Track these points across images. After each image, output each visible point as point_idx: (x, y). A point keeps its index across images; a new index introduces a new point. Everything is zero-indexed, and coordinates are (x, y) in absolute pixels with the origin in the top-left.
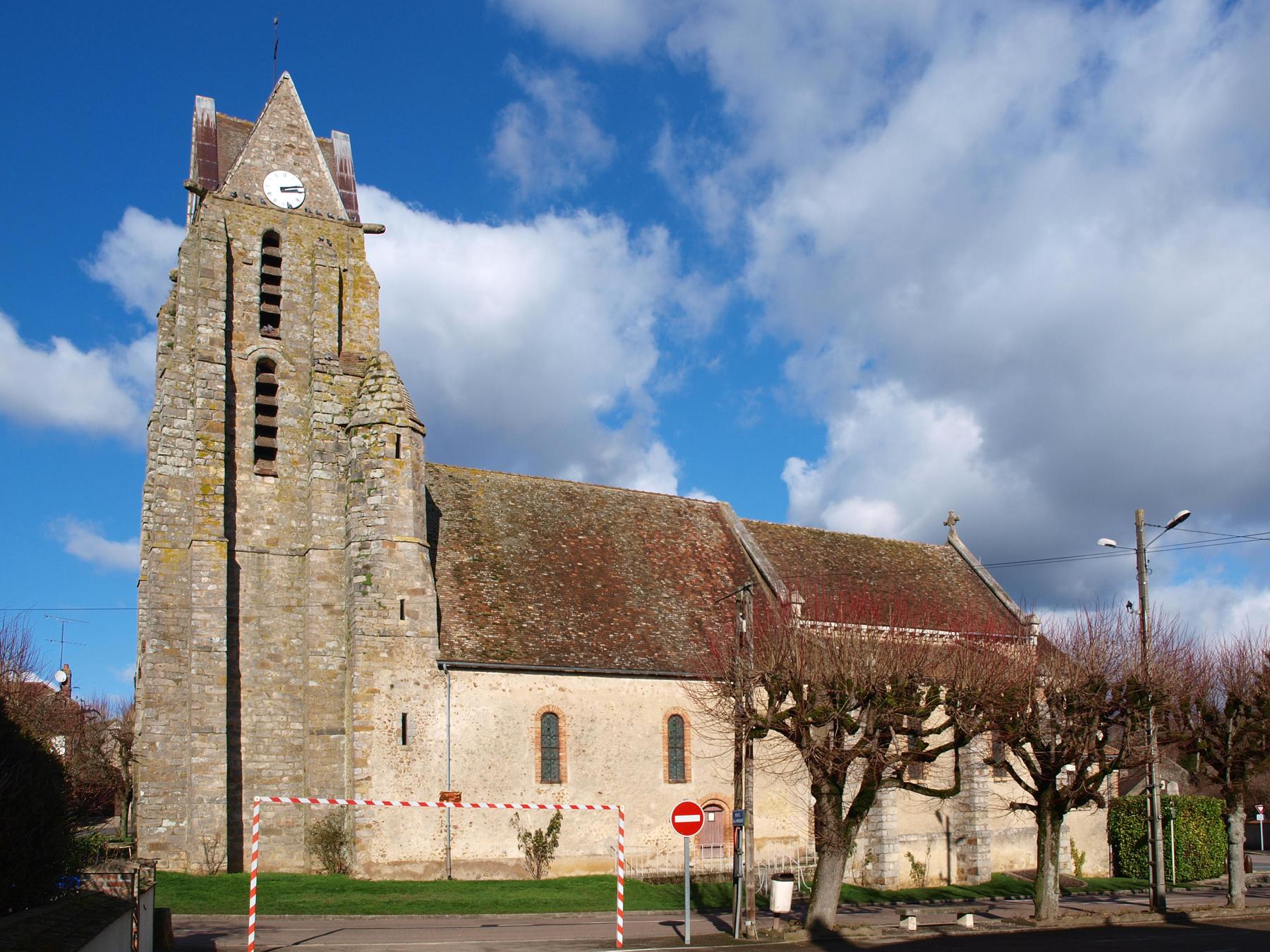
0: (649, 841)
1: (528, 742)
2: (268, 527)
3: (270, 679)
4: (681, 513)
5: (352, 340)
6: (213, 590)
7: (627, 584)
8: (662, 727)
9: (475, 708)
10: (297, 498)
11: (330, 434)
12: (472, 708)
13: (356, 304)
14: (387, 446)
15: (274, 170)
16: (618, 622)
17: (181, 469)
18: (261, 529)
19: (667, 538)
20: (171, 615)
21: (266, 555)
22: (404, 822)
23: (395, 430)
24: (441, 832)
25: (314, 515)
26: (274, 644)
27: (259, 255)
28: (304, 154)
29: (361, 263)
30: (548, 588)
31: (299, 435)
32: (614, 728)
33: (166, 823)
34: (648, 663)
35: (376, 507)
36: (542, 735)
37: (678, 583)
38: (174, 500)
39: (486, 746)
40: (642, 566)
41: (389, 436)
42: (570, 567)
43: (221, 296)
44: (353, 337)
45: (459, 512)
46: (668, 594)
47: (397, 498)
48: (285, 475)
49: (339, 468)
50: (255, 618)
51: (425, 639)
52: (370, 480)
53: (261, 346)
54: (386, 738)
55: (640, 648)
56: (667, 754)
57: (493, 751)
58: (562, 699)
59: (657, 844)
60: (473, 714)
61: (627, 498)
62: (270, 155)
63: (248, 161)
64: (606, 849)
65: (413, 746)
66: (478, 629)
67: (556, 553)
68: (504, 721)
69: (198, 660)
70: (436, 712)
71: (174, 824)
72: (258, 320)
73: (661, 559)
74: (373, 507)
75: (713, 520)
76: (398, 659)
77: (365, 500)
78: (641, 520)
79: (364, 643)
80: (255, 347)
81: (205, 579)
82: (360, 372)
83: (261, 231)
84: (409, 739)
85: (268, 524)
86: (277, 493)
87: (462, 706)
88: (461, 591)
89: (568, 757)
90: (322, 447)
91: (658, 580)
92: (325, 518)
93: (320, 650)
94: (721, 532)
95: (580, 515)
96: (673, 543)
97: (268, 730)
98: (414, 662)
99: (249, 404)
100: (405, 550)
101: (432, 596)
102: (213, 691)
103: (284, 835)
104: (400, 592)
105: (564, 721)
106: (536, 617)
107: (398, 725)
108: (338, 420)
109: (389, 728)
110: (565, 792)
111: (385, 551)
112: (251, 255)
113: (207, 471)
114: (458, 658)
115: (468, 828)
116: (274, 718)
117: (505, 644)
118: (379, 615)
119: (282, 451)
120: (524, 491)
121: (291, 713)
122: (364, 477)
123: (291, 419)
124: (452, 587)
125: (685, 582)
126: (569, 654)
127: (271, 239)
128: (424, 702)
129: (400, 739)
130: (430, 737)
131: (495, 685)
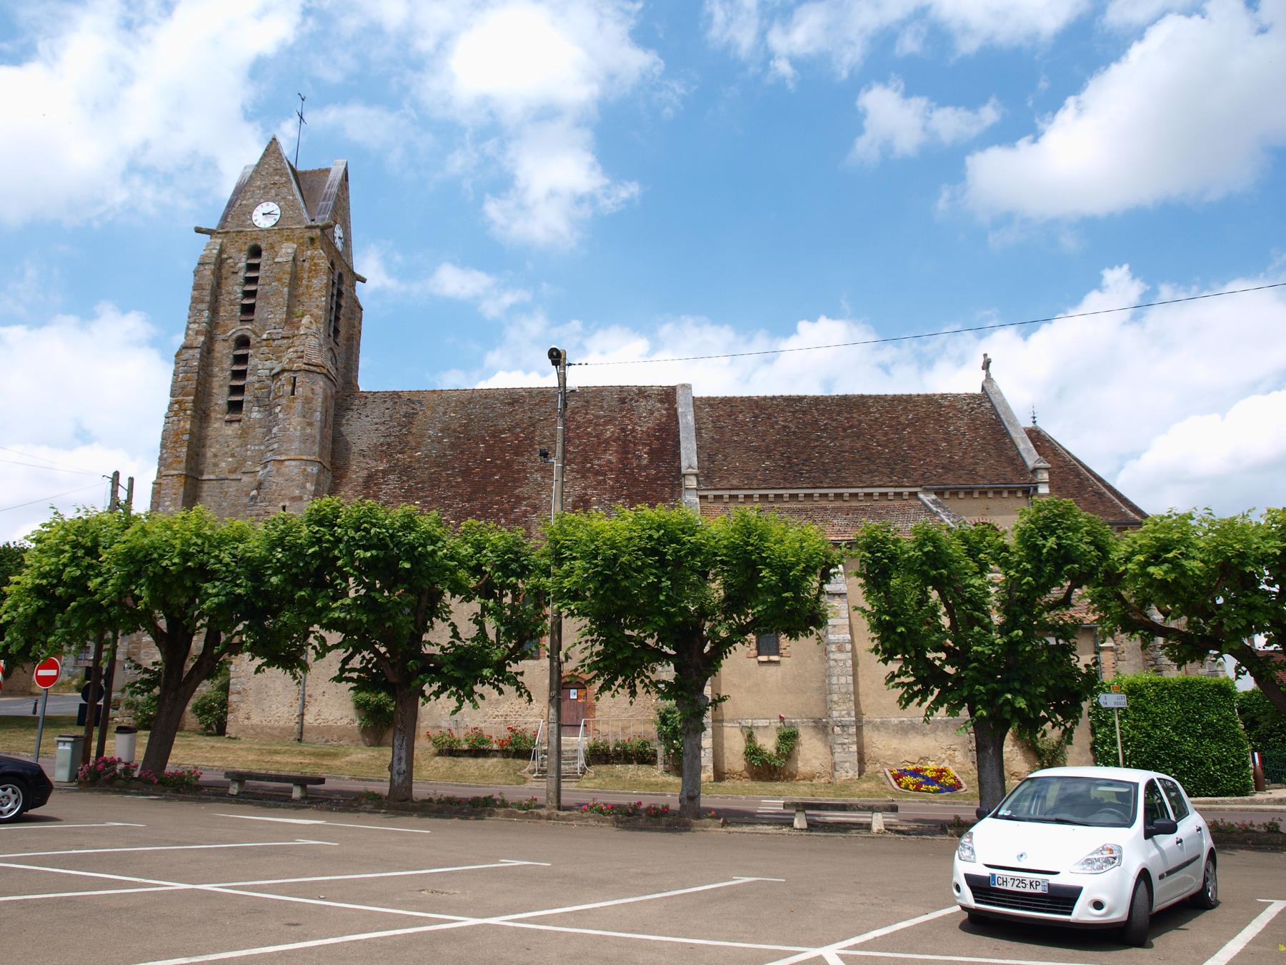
2: (230, 459)
18: (226, 461)
22: (267, 690)
63: (245, 202)
80: (234, 330)
104: (282, 500)
115: (320, 698)
127: (256, 252)
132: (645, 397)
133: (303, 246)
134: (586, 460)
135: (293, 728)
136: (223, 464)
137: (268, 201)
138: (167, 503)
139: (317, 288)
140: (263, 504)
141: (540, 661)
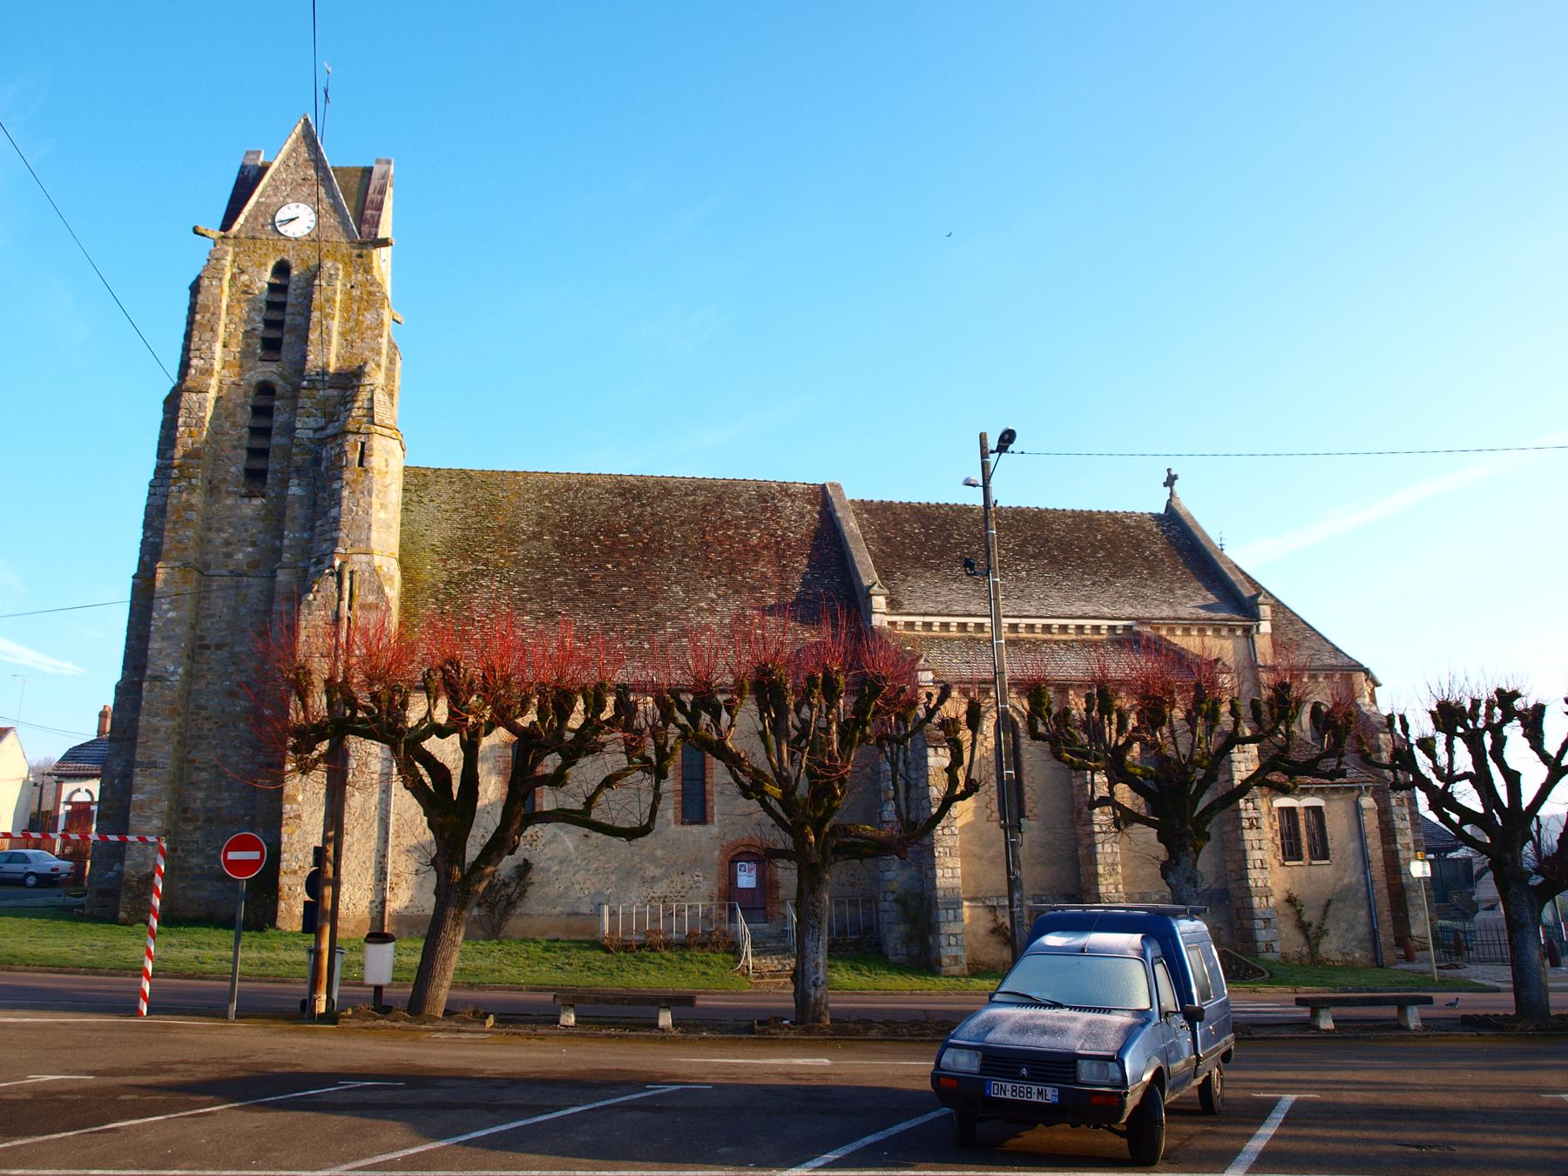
0: (653, 898)
2: (250, 549)
3: (238, 709)
6: (173, 618)
21: (245, 579)
25: (286, 533)
48: (273, 495)
50: (228, 644)
61: (699, 487)
64: (593, 907)
91: (708, 577)
110: (540, 834)
132: (790, 496)
134: (733, 570)
136: (240, 556)
137: (297, 201)
138: (165, 607)
141: (707, 826)
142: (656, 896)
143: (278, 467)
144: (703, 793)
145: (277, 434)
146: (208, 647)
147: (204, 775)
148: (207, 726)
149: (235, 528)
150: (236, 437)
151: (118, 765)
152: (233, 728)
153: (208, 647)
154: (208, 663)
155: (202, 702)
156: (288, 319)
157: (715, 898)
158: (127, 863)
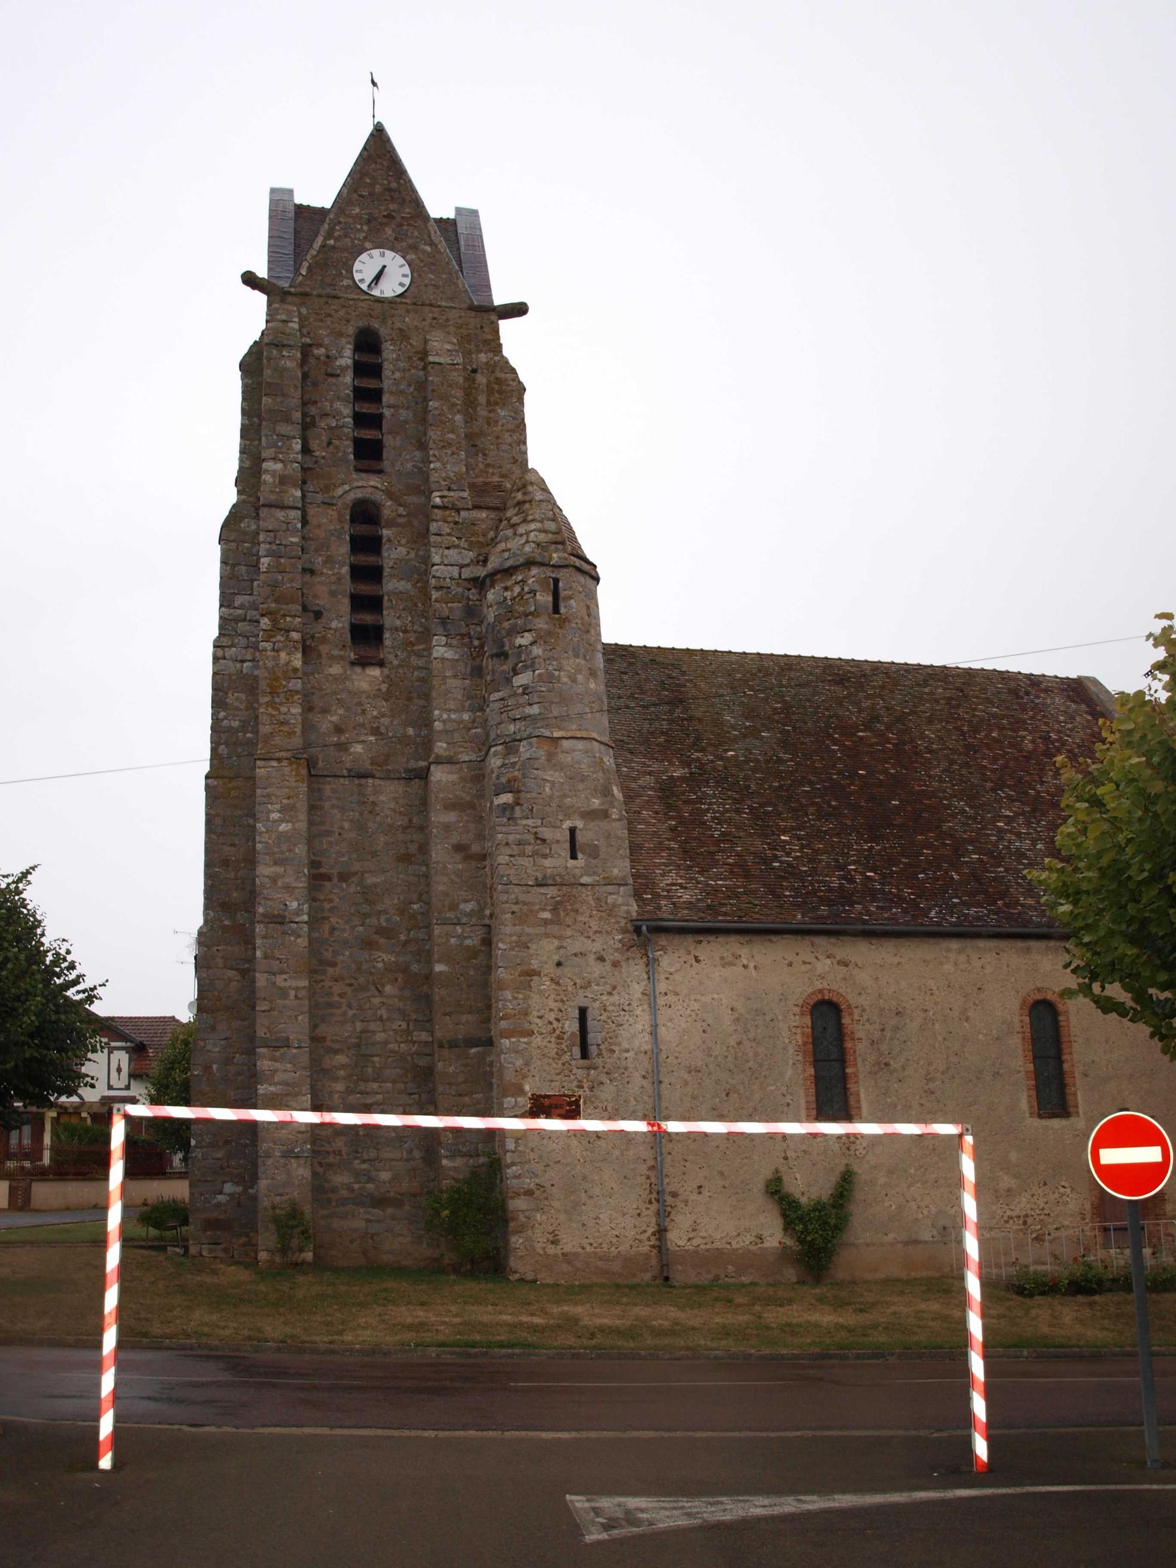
0: (1010, 1217)
1: (791, 1051)
2: (372, 738)
3: (380, 965)
4: (1021, 694)
5: (488, 466)
6: (287, 832)
7: (942, 799)
8: (1018, 1020)
9: (699, 997)
10: (415, 695)
11: (457, 594)
12: (693, 998)
13: (492, 415)
14: (538, 597)
15: (367, 250)
16: (932, 855)
17: (245, 665)
19: (1002, 729)
20: (232, 875)
21: (370, 781)
23: (549, 573)
24: (650, 1202)
25: (437, 712)
26: (385, 912)
27: (350, 362)
28: (408, 225)
29: (496, 358)
30: (812, 809)
31: (416, 605)
32: (937, 1026)
33: (229, 1188)
34: (987, 915)
35: (525, 687)
36: (814, 1038)
37: (1027, 794)
38: (237, 709)
39: (720, 1059)
40: (964, 772)
41: (543, 582)
42: (847, 778)
43: (294, 418)
44: (489, 461)
45: (666, 708)
46: (1011, 811)
47: (557, 673)
48: (396, 662)
49: (471, 642)
51: (610, 888)
52: (516, 651)
53: (356, 484)
54: (553, 1049)
55: (971, 894)
56: (1031, 1067)
57: (732, 1067)
58: (845, 979)
59: (1025, 1223)
60: (696, 1006)
62: (361, 230)
64: (935, 1232)
65: (599, 1061)
66: (699, 872)
67: (823, 758)
68: (749, 1017)
69: (265, 937)
70: (635, 1004)
71: (239, 1189)
72: (350, 450)
73: (994, 760)
74: (520, 690)
75: (1074, 702)
76: (569, 920)
77: (509, 681)
78: (958, 706)
79: (513, 896)
80: (347, 487)
81: (275, 816)
82: (496, 503)
83: (351, 330)
84: (593, 1050)
85: (372, 734)
86: (384, 690)
87: (677, 994)
88: (672, 818)
89: (861, 1076)
90: (446, 613)
92: (453, 716)
93: (450, 915)
94: (1089, 718)
95: (857, 704)
96: (1012, 737)
97: (379, 1043)
98: (595, 925)
99: (342, 565)
100: (574, 751)
101: (619, 820)
102: (287, 984)
103: (407, 1207)
104: (568, 816)
105: (851, 1014)
106: (795, 851)
107: (572, 1026)
108: (467, 573)
109: (557, 1032)
111: (541, 754)
112: (338, 363)
113: (276, 658)
114: (665, 916)
115: (695, 1197)
116: (388, 1024)
117: (745, 893)
118: (535, 854)
119: (391, 629)
120: (767, 674)
121: (414, 1016)
122: (507, 648)
123: (402, 583)
124: (657, 813)
125: (1039, 792)
126: (852, 905)
127: (368, 343)
128: (614, 988)
129: (577, 1051)
130: (626, 1045)
131: (730, 959)
133: (469, 342)
135: (647, 1256)
136: (358, 748)
139: (510, 427)
140: (530, 822)
142: (1013, 1214)
143: (398, 623)
144: (844, 1078)
145: (392, 576)
146: (328, 878)
147: (341, 1059)
148: (337, 988)
149: (348, 709)
150: (333, 579)
151: (215, 1045)
152: (376, 993)
153: (328, 878)
154: (331, 901)
155: (328, 955)
156: (387, 412)
157: (1088, 1216)
158: (263, 1183)
